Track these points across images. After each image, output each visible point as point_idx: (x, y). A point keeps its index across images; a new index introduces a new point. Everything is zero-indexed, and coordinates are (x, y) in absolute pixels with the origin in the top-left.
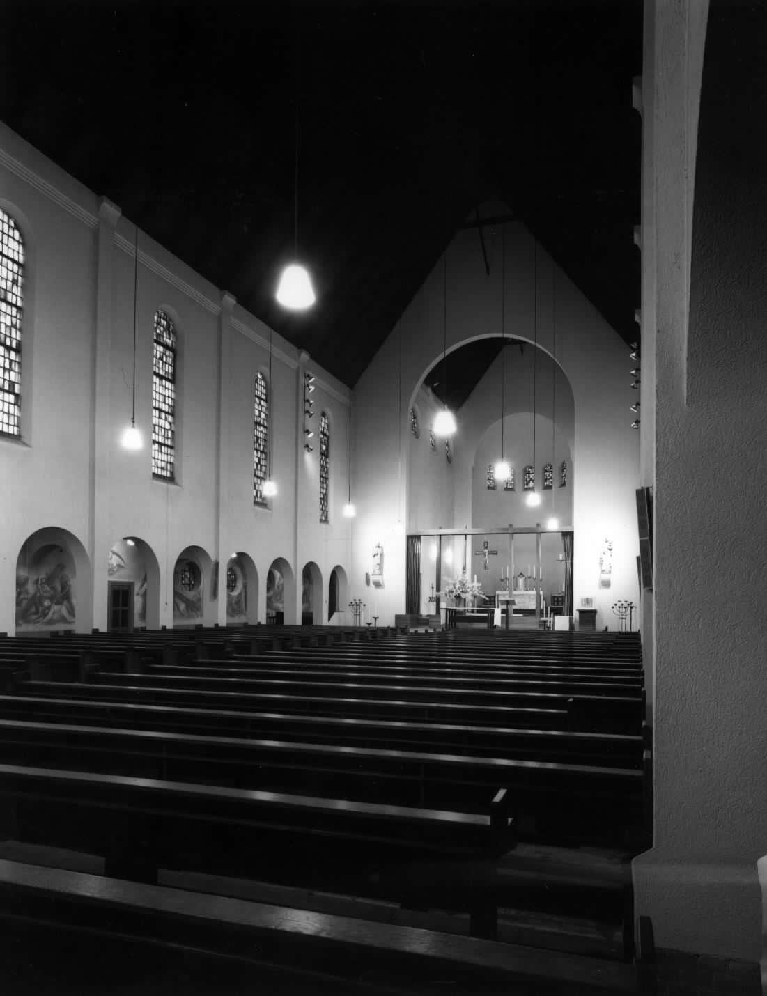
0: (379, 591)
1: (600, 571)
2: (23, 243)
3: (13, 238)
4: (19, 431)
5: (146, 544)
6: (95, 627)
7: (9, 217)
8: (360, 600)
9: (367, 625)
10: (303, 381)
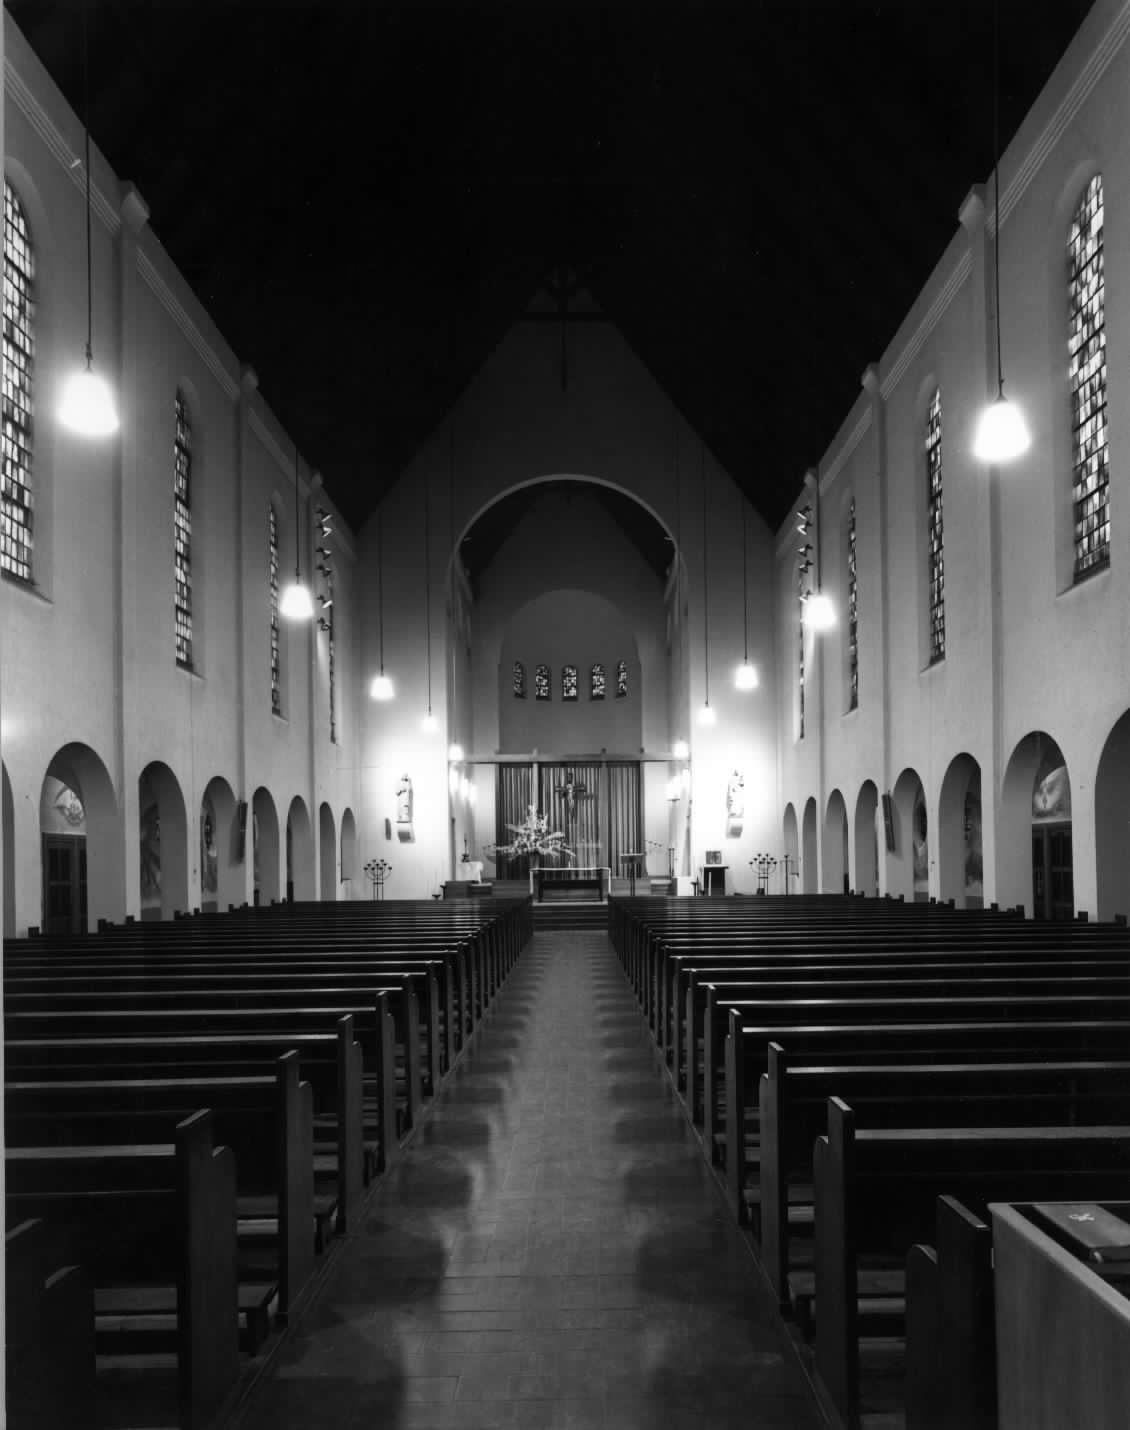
0: (406, 846)
1: (726, 814)
2: (28, 242)
3: (18, 230)
4: (30, 574)
6: (129, 914)
7: (14, 194)
8: (382, 861)
9: (433, 898)
10: (316, 517)
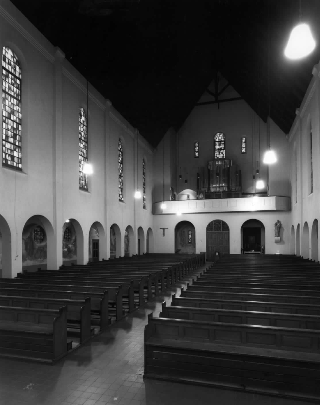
5: (119, 228)
